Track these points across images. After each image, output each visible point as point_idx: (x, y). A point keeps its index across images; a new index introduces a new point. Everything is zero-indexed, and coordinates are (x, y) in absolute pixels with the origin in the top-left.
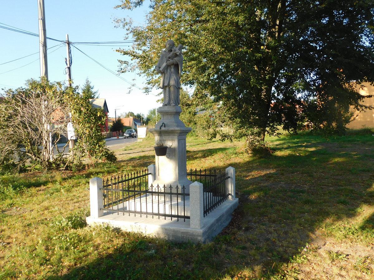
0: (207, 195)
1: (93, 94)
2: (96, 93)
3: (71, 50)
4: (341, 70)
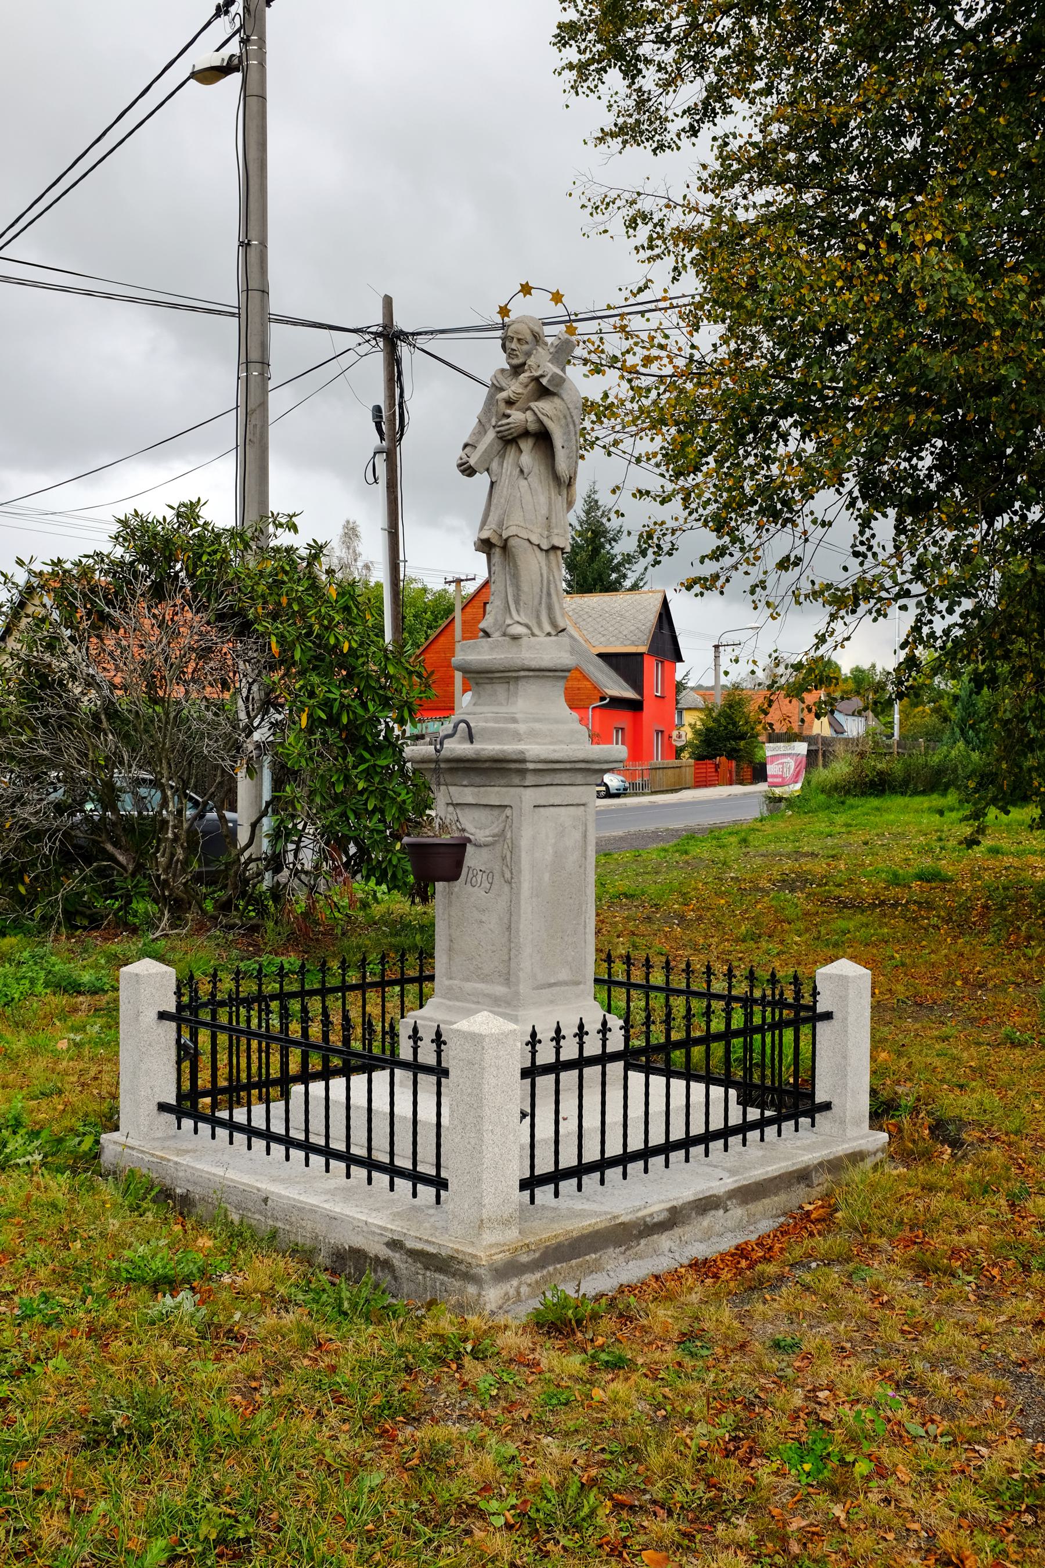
0: (657, 1105)
1: (616, 569)
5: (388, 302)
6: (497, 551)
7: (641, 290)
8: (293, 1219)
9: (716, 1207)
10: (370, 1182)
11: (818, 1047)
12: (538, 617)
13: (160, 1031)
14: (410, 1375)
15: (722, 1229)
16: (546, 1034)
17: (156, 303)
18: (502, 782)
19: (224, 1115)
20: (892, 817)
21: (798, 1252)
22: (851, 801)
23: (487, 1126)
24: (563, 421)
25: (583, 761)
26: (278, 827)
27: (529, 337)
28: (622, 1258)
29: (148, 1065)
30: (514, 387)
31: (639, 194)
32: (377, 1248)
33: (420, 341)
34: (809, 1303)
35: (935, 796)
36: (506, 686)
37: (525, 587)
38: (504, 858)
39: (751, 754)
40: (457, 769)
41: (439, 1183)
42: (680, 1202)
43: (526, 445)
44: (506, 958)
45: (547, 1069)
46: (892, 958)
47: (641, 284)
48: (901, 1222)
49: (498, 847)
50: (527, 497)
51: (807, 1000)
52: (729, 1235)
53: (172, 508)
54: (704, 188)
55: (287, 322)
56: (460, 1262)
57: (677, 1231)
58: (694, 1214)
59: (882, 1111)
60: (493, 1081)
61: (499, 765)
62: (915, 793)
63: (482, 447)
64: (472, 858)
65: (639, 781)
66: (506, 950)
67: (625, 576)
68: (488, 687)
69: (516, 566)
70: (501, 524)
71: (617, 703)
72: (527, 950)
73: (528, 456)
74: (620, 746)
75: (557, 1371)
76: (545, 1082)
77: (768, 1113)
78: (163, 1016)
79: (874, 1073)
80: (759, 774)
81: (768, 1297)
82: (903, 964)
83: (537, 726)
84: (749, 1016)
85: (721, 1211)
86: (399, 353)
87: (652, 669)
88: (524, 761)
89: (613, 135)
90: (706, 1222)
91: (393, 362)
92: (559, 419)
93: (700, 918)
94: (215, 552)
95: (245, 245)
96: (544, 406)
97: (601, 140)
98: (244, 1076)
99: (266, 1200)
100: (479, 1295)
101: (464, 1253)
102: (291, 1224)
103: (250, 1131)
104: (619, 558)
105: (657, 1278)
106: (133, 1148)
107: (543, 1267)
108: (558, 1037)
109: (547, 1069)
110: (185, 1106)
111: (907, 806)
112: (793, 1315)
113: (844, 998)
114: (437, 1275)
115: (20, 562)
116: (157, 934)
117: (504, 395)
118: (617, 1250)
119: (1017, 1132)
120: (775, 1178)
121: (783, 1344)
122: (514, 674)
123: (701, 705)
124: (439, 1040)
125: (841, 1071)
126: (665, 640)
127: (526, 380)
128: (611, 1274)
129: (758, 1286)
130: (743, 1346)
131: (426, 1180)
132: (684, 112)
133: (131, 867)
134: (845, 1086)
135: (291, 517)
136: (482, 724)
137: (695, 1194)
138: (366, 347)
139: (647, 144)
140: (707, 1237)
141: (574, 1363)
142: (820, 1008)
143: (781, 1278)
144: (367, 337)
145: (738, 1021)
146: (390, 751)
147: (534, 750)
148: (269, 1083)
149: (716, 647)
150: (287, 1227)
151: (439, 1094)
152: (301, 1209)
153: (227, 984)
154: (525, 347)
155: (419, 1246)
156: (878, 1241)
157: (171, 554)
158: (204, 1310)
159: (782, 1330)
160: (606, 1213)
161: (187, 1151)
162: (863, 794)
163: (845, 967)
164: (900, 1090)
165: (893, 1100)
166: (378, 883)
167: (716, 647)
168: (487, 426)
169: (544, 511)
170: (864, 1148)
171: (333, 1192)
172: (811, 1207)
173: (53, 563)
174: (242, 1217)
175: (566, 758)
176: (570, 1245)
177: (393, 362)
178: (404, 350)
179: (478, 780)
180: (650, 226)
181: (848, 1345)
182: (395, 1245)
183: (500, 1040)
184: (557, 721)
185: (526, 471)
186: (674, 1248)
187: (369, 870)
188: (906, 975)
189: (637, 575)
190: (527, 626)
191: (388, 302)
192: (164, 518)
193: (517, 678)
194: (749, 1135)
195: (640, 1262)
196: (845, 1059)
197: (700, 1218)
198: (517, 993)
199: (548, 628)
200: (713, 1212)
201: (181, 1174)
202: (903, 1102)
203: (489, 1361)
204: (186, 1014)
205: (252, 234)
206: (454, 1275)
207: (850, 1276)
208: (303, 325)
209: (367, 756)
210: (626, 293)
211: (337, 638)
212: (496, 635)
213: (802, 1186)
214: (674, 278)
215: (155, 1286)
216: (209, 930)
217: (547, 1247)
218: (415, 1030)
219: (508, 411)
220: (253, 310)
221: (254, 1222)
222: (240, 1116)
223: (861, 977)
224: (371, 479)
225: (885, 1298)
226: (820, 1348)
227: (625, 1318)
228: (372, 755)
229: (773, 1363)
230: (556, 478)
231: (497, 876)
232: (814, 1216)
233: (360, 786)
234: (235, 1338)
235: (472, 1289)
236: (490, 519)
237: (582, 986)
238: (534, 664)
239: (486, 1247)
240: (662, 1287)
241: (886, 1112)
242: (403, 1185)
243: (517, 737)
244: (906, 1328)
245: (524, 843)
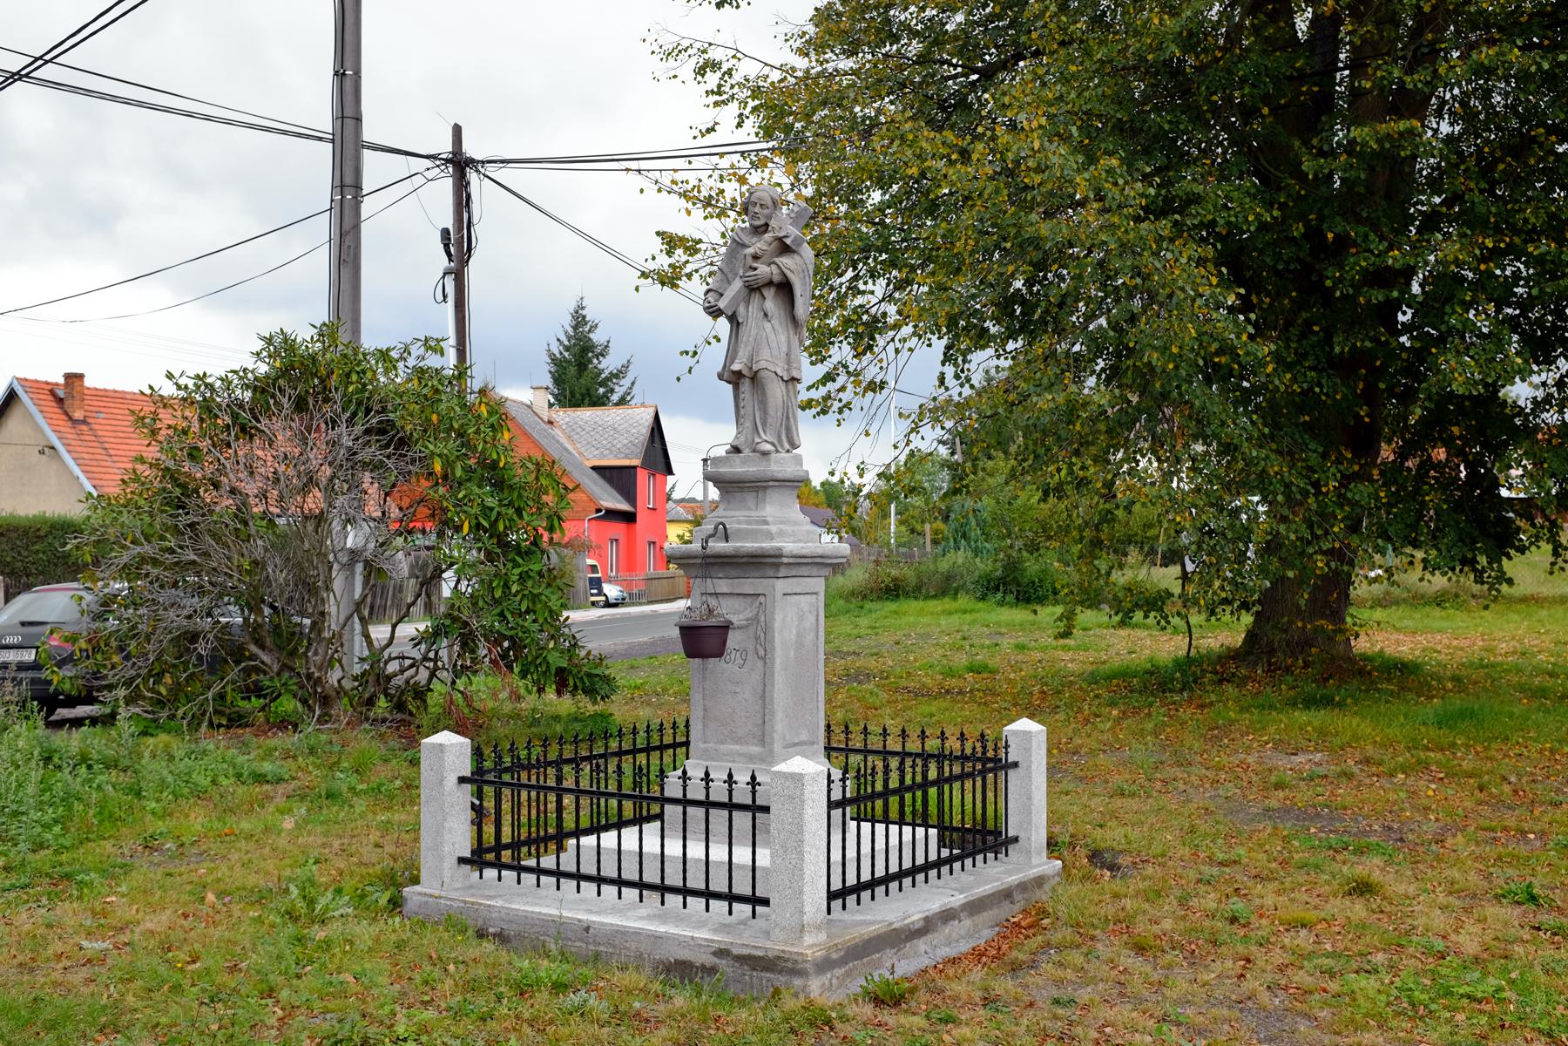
0: (894, 841)
1: (603, 384)
2: (617, 376)
3: (469, 196)
4: (1338, 294)
5: (457, 130)
6: (746, 386)
7: (709, 131)
9: (953, 918)
12: (779, 437)
19: (532, 862)
20: (912, 619)
22: (868, 605)
23: (807, 849)
27: (770, 203)
29: (448, 824)
32: (703, 958)
33: (490, 170)
35: (946, 600)
37: (771, 412)
38: (757, 638)
40: (713, 564)
47: (710, 125)
48: (1107, 919)
49: (752, 630)
50: (772, 337)
57: (929, 937)
59: (1052, 845)
62: (927, 597)
64: (733, 639)
65: (635, 591)
66: (759, 716)
67: (612, 391)
69: (764, 394)
71: (612, 514)
72: (779, 715)
73: (771, 302)
77: (955, 852)
78: (462, 780)
84: (940, 769)
87: (644, 483)
88: (781, 556)
91: (461, 186)
95: (339, 75)
96: (786, 261)
98: (524, 830)
99: (587, 929)
103: (559, 874)
104: (607, 372)
110: (478, 859)
111: (922, 609)
113: (1028, 750)
115: (170, 376)
117: (750, 251)
119: (1163, 855)
123: (690, 518)
125: (1027, 811)
126: (657, 455)
133: (276, 668)
134: (1030, 822)
135: (438, 341)
145: (933, 774)
147: (789, 547)
148: (547, 839)
149: (705, 460)
152: (624, 933)
153: (537, 751)
155: (745, 952)
162: (879, 598)
163: (1025, 724)
167: (705, 460)
169: (784, 349)
171: (649, 918)
173: (197, 376)
177: (461, 186)
178: (473, 177)
179: (733, 573)
180: (718, 74)
182: (721, 953)
184: (795, 523)
189: (623, 389)
191: (457, 130)
193: (766, 488)
196: (1029, 801)
198: (771, 752)
199: (787, 446)
201: (495, 915)
205: (347, 64)
206: (780, 972)
212: (746, 452)
220: (347, 137)
222: (548, 862)
224: (440, 297)
231: (751, 653)
232: (1024, 923)
235: (797, 982)
238: (780, 476)
239: (811, 945)
243: (770, 536)
245: (777, 625)
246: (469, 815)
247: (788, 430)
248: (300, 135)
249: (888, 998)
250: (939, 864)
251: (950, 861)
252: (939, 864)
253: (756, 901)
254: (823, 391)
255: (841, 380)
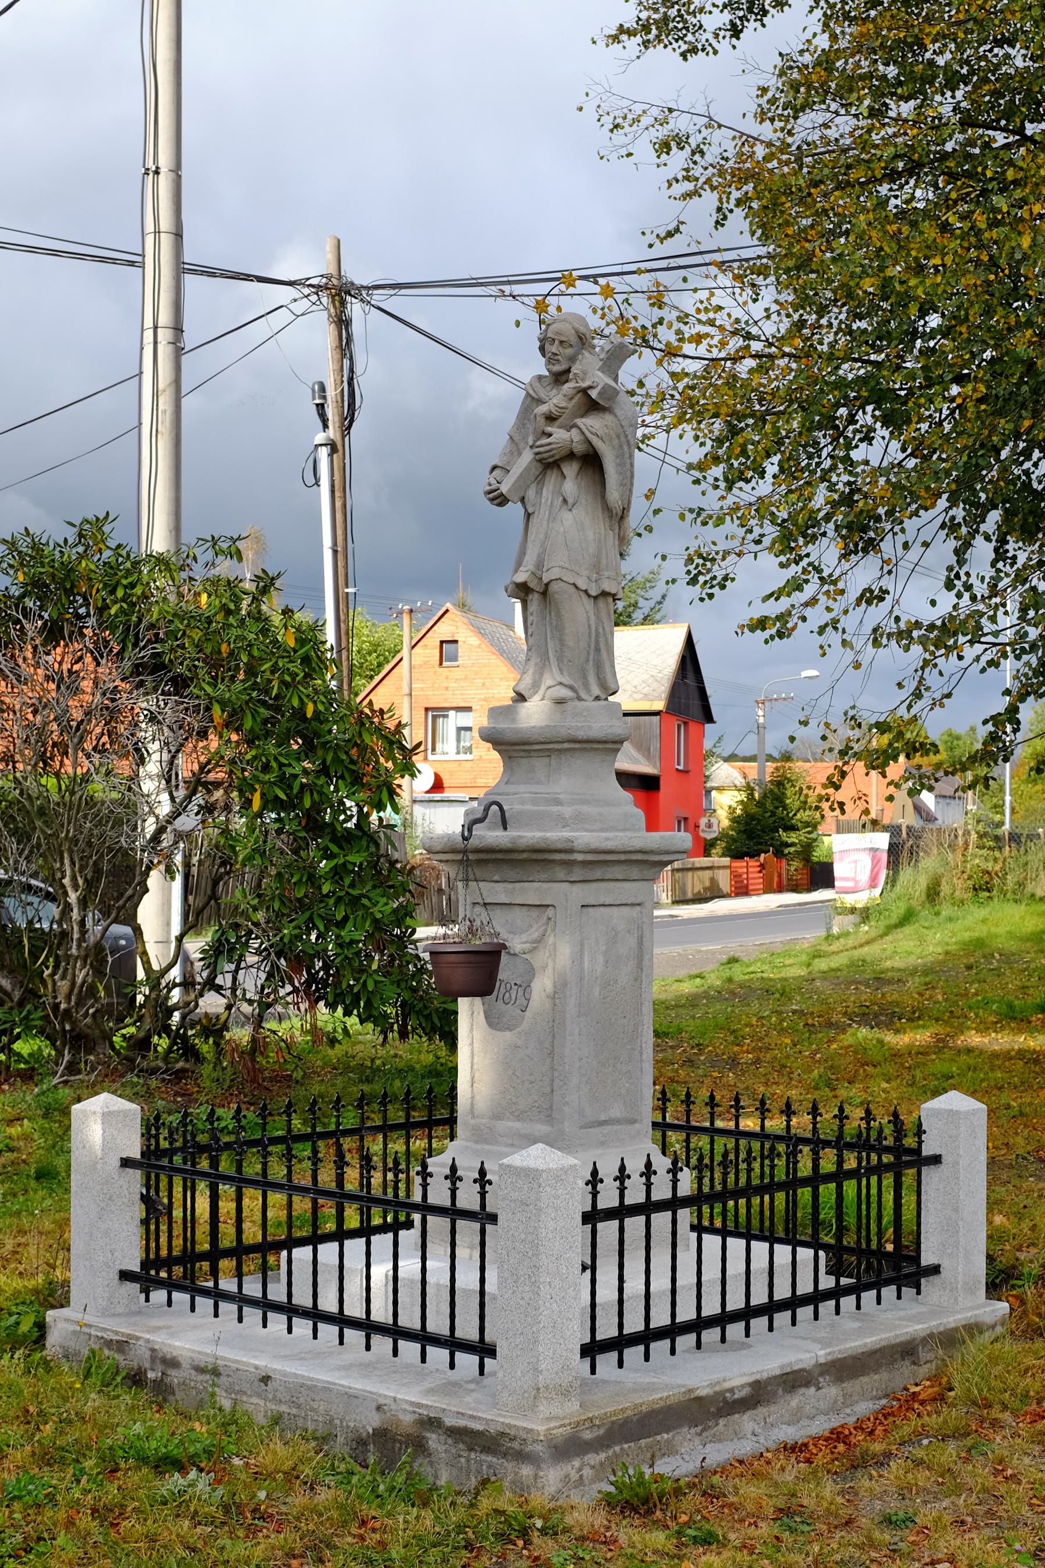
6: (534, 599)
7: (670, 235)
8: (302, 1400)
9: (807, 1384)
10: (395, 1353)
11: (923, 1198)
12: (584, 677)
13: (121, 1182)
14: (471, 1552)
15: (814, 1411)
16: (608, 1170)
17: (32, 249)
18: (543, 876)
21: (907, 1430)
24: (616, 442)
25: (640, 852)
26: (219, 940)
27: (574, 340)
28: (697, 1441)
29: (104, 1224)
30: (556, 399)
31: (671, 110)
33: (378, 297)
34: (922, 1477)
36: (547, 760)
37: (570, 642)
39: (808, 848)
40: (486, 861)
41: (484, 1350)
42: (765, 1375)
43: (570, 470)
44: (549, 1089)
45: (610, 1214)
46: (1008, 1107)
47: (671, 227)
51: (910, 1142)
52: (822, 1418)
53: (74, 526)
54: (762, 116)
55: (203, 273)
56: (513, 1439)
57: (761, 1411)
58: (780, 1392)
59: (1000, 1280)
60: (551, 1225)
61: (539, 856)
63: (516, 471)
68: (525, 761)
69: (559, 616)
70: (540, 564)
73: (571, 482)
74: (682, 833)
75: (639, 1546)
76: (608, 1230)
77: (844, 1281)
79: (990, 1237)
80: (821, 875)
81: (874, 1472)
82: (1021, 1114)
83: (585, 809)
85: (812, 1390)
86: (348, 311)
89: (631, 33)
90: (795, 1401)
91: (343, 323)
92: (611, 440)
93: (757, 1061)
94: (132, 586)
96: (592, 423)
97: (615, 38)
100: (536, 1477)
101: (517, 1428)
102: (299, 1407)
105: (741, 1462)
106: (90, 1326)
107: (609, 1446)
108: (622, 1176)
109: (610, 1214)
110: (146, 1277)
112: (904, 1492)
114: (484, 1457)
116: (56, 1081)
117: (543, 409)
118: (693, 1430)
120: (876, 1352)
121: (894, 1518)
122: (556, 746)
124: (482, 1179)
127: (571, 392)
128: (687, 1458)
129: (858, 1463)
130: (849, 1522)
131: (467, 1347)
132: (725, 6)
133: (17, 995)
136: (517, 807)
137: (782, 1367)
138: (305, 304)
139: (675, 45)
140: (795, 1418)
141: (659, 1538)
142: (927, 1151)
143: (888, 1455)
144: (306, 291)
145: (828, 1165)
146: (364, 843)
150: (294, 1411)
151: (483, 1244)
152: (311, 1387)
154: (569, 351)
155: (462, 1423)
156: (1000, 1416)
157: (73, 586)
158: (220, 1491)
159: (893, 1506)
160: (678, 1386)
161: (159, 1328)
163: (954, 1101)
164: (1022, 1256)
165: (1014, 1267)
166: (347, 1013)
168: (521, 445)
170: (980, 1319)
171: (346, 1368)
172: (917, 1389)
174: (235, 1402)
175: (621, 848)
176: (638, 1420)
177: (343, 323)
178: (355, 309)
179: (512, 874)
181: (969, 1519)
182: (432, 1423)
183: (560, 1176)
185: (570, 501)
186: (758, 1431)
187: (336, 995)
188: (1026, 1126)
190: (571, 688)
192: (66, 540)
194: (843, 1301)
195: (718, 1446)
196: (956, 1215)
197: (788, 1397)
199: (596, 691)
200: (803, 1390)
202: (1026, 1270)
203: (560, 1537)
204: (154, 1161)
206: (505, 1455)
207: (969, 1451)
208: (222, 276)
209: (335, 849)
210: (651, 238)
211: (300, 699)
213: (907, 1363)
214: (717, 222)
215: (157, 1467)
216: (122, 1076)
217: (613, 1423)
218: (454, 1168)
219: (549, 429)
221: (251, 1408)
223: (974, 1112)
225: (1009, 1472)
226: (937, 1520)
227: (711, 1494)
228: (341, 847)
229: (885, 1536)
230: (607, 508)
232: (919, 1389)
233: (325, 889)
234: (262, 1518)
235: (526, 1471)
236: (527, 558)
237: (637, 1125)
238: (581, 734)
240: (747, 1467)
241: (1005, 1281)
242: (438, 1355)
244: (1034, 1501)
246: (139, 1211)
247: (599, 667)
248: (103, 260)
249: (638, 1503)
250: (816, 1298)
251: (836, 1294)
252: (816, 1298)
253: (484, 1350)
254: (784, 604)
255: (810, 590)
